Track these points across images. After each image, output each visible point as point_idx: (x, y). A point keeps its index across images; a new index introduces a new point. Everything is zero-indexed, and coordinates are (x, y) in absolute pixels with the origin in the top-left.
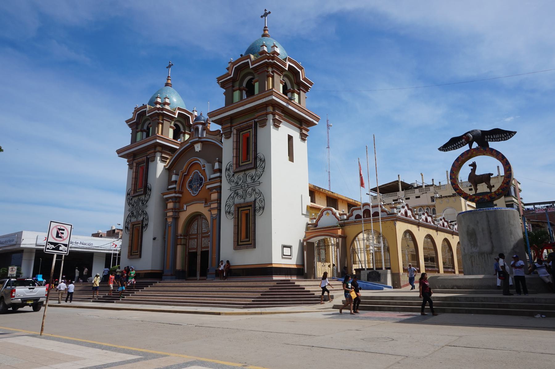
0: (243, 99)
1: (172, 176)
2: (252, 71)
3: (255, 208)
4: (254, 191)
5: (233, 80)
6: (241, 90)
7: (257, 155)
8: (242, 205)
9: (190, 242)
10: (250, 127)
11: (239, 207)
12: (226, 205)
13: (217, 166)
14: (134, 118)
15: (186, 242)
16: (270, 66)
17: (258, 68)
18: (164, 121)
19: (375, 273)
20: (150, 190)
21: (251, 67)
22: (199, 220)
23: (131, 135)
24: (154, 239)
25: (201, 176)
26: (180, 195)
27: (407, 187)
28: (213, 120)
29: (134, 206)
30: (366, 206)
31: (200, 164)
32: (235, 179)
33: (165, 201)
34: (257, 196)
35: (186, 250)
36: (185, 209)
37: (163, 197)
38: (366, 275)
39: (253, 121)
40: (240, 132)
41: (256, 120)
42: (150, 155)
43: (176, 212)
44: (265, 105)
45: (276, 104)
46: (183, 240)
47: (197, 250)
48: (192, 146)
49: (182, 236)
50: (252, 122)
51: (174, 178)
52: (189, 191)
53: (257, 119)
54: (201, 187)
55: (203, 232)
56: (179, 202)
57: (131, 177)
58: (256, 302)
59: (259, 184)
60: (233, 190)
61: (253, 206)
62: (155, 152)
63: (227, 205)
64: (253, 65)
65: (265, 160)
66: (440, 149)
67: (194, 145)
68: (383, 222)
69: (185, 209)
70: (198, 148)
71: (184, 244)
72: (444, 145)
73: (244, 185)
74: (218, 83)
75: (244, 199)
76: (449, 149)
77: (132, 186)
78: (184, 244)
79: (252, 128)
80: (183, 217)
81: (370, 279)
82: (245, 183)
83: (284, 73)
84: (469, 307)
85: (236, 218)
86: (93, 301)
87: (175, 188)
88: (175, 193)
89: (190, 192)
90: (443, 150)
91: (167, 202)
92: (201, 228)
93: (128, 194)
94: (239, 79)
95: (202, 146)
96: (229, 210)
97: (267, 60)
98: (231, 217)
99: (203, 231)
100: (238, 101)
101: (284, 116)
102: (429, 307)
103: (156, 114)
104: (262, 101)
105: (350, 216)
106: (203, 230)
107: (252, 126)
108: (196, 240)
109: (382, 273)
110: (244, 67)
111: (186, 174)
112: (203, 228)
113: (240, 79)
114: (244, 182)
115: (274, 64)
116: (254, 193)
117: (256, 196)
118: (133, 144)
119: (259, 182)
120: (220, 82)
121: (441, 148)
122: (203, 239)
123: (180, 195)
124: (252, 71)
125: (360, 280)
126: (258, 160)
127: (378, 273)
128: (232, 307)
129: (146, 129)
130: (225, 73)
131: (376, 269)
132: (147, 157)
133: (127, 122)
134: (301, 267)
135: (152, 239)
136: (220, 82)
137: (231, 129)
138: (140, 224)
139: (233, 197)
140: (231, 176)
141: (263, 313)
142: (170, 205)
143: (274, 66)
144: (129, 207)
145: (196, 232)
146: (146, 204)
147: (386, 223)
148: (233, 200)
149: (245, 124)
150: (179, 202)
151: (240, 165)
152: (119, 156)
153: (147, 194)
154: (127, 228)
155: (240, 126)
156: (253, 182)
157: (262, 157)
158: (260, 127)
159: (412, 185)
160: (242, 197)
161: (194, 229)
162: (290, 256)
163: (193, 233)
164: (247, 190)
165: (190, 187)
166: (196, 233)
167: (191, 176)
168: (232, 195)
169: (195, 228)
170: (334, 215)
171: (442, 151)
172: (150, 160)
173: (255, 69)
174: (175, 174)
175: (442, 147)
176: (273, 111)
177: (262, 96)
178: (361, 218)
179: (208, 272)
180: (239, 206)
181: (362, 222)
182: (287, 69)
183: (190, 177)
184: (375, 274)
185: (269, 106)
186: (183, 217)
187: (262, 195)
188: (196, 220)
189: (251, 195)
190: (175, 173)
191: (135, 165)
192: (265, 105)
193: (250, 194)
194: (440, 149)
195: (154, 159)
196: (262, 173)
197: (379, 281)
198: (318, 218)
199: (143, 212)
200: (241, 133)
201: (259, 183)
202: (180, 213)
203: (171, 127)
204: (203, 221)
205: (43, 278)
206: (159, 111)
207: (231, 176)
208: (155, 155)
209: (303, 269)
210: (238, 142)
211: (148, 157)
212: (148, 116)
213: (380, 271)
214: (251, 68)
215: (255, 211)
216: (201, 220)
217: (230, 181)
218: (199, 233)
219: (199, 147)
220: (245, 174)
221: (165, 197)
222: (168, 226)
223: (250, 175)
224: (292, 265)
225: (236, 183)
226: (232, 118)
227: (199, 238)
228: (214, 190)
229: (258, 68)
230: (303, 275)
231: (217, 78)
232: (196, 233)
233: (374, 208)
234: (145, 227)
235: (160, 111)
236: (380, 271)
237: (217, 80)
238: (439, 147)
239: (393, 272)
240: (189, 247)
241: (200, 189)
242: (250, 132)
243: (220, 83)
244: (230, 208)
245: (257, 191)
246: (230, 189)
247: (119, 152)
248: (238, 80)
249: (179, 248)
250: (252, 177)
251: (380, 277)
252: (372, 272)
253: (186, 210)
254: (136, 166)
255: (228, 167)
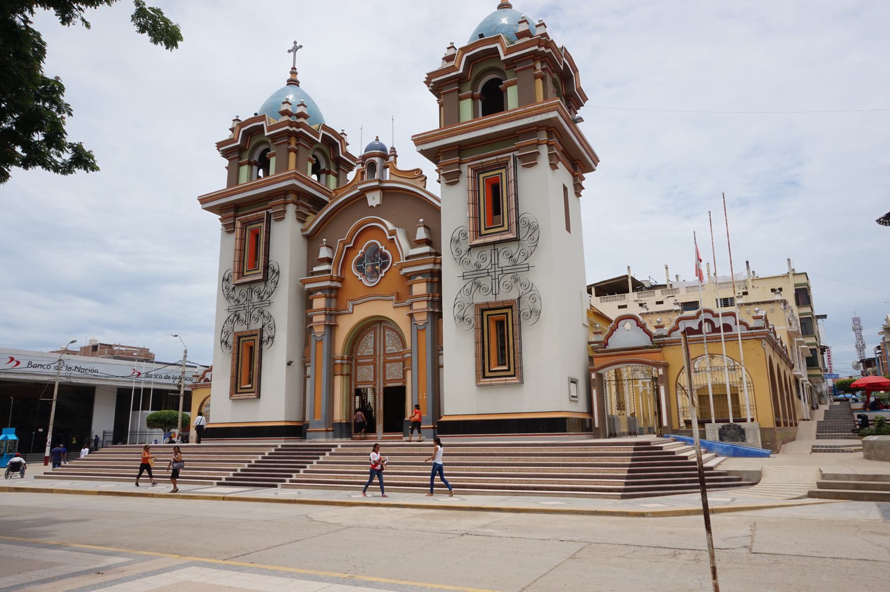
0: (509, 109)
1: (320, 250)
2: (503, 67)
3: (262, 338)
4: (262, 313)
5: (240, 150)
6: (473, 98)
7: (270, 264)
8: (491, 306)
9: (358, 369)
10: (259, 220)
11: (483, 310)
12: (222, 331)
13: (421, 234)
14: (236, 138)
15: (351, 370)
16: (539, 59)
17: (275, 137)
18: (301, 147)
19: (734, 427)
20: (278, 273)
21: (266, 134)
22: (378, 331)
23: (226, 171)
24: (289, 364)
25: (384, 250)
26: (339, 285)
27: (638, 286)
28: (424, 149)
29: (239, 301)
30: (633, 320)
31: (382, 230)
32: (237, 295)
33: (307, 298)
34: (265, 321)
35: (351, 385)
36: (350, 310)
37: (400, 273)
38: (717, 431)
39: (265, 211)
40: (246, 226)
41: (271, 211)
42: (273, 208)
43: (331, 315)
44: (536, 128)
45: (301, 192)
46: (345, 366)
47: (405, 382)
48: (361, 197)
49: (344, 360)
50: (510, 156)
51: (324, 253)
52: (358, 277)
53: (518, 152)
54: (384, 271)
55: (387, 352)
56: (336, 297)
57: (234, 248)
58: (651, 484)
59: (527, 269)
60: (232, 310)
61: (259, 335)
62: (286, 204)
63: (223, 332)
64: (507, 55)
65: (279, 271)
66: (879, 221)
67: (365, 195)
68: (744, 341)
69: (350, 310)
70: (374, 199)
71: (347, 375)
72: (886, 214)
73: (247, 305)
74: (218, 149)
75: (248, 325)
76: (886, 223)
77: (234, 264)
78: (347, 375)
79: (263, 222)
80: (346, 325)
81: (724, 437)
82: (497, 265)
83: (315, 146)
84: (589, 473)
85: (478, 329)
86: (219, 484)
87: (329, 271)
88: (331, 280)
89: (360, 278)
90: (884, 224)
91: (410, 282)
92: (382, 345)
93: (225, 280)
94: (470, 77)
95: (381, 197)
96: (225, 339)
97: (537, 47)
98: (465, 326)
99: (388, 350)
100: (245, 182)
101: (312, 208)
102: (698, 478)
103: (287, 133)
104: (534, 119)
105: (674, 331)
106: (387, 348)
107: (264, 219)
108: (372, 367)
109: (747, 428)
110: (483, 57)
111: (351, 245)
112: (387, 345)
113: (250, 148)
114: (493, 263)
115: (546, 57)
116: (262, 316)
117: (264, 321)
118: (280, 172)
119: (527, 266)
120: (221, 149)
121: (882, 220)
122: (388, 365)
123: (339, 285)
124: (503, 67)
125: (706, 439)
126: (270, 271)
127: (739, 427)
128: (615, 497)
129: (257, 160)
130: (228, 138)
131: (734, 422)
132: (267, 212)
133: (219, 145)
134: (587, 417)
135: (285, 364)
136: (221, 149)
137: (235, 220)
138: (257, 335)
139: (232, 320)
140: (230, 290)
141: (716, 509)
142: (319, 303)
143: (547, 59)
144: (229, 305)
145: (371, 352)
146: (269, 299)
147: (746, 343)
148: (233, 324)
149: (493, 160)
150: (336, 297)
151: (245, 274)
152: (206, 209)
153: (270, 281)
154: (226, 343)
155: (482, 163)
156: (261, 301)
157: (276, 268)
158: (274, 220)
159: (644, 283)
160: (244, 322)
161: (367, 347)
162: (576, 397)
163: (365, 354)
164: (251, 312)
165: (360, 270)
166: (372, 354)
167: (362, 251)
168: (231, 317)
169: (369, 344)
170: (641, 328)
171: (883, 224)
172: (272, 218)
173: (273, 138)
174: (326, 246)
175: (883, 218)
176: (298, 200)
177: (533, 110)
178: (720, 332)
179: (308, 428)
180: (240, 334)
181: (703, 340)
182: (319, 141)
183: (360, 251)
184: (734, 429)
185: (542, 130)
186: (346, 325)
187: (272, 319)
188: (371, 330)
189: (257, 320)
190: (325, 244)
191: (238, 224)
192: (536, 128)
193: (508, 286)
194: (879, 221)
195: (284, 215)
196: (273, 289)
197: (742, 441)
198: (609, 333)
199: (262, 313)
200: (248, 228)
201: (269, 303)
202: (338, 316)
203: (310, 160)
204: (387, 333)
205: (73, 440)
206: (291, 127)
207: (463, 253)
208: (285, 208)
209: (591, 421)
210: (242, 239)
211: (271, 211)
212: (268, 136)
213: (743, 425)
214: (502, 59)
215: (261, 343)
216: (382, 330)
217: (460, 261)
218: (378, 354)
219: (375, 198)
220: (494, 249)
221: (307, 286)
222: (316, 341)
223: (257, 291)
224: (572, 413)
225: (236, 300)
226: (461, 149)
227: (378, 363)
228: (319, 293)
229: (275, 137)
230: (592, 431)
231: (427, 74)
232: (372, 354)
233: (724, 317)
234: (267, 342)
235: (294, 129)
236: (743, 425)
237: (427, 76)
238: (878, 218)
239: (761, 427)
240: (358, 378)
241: (383, 275)
242: (260, 227)
243: (221, 151)
244: (227, 336)
245: (266, 314)
246: (228, 309)
247: (203, 200)
248: (248, 150)
249: (338, 380)
250: (259, 294)
251: (744, 434)
252: (728, 426)
253: (353, 313)
254: (242, 228)
255: (226, 275)
